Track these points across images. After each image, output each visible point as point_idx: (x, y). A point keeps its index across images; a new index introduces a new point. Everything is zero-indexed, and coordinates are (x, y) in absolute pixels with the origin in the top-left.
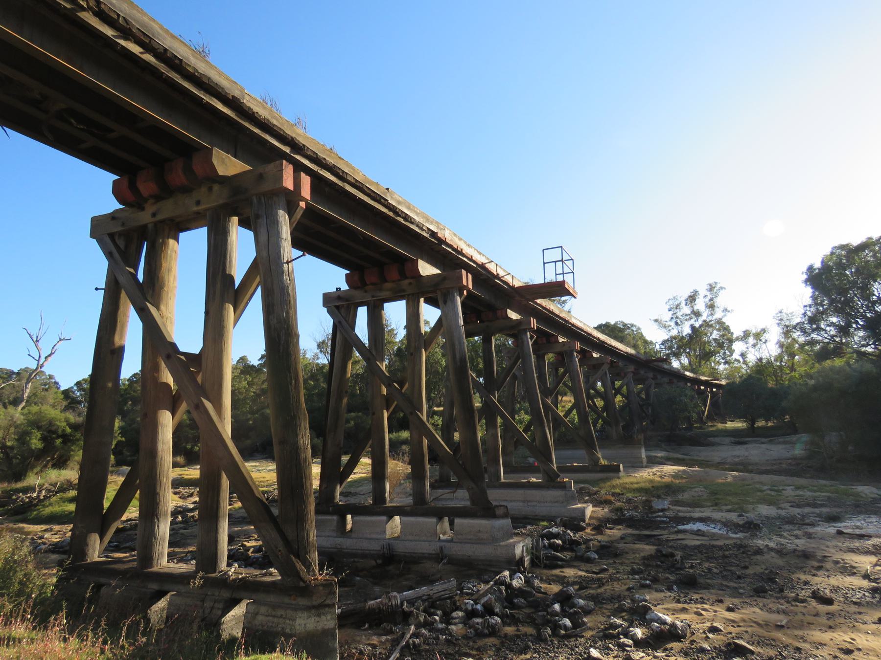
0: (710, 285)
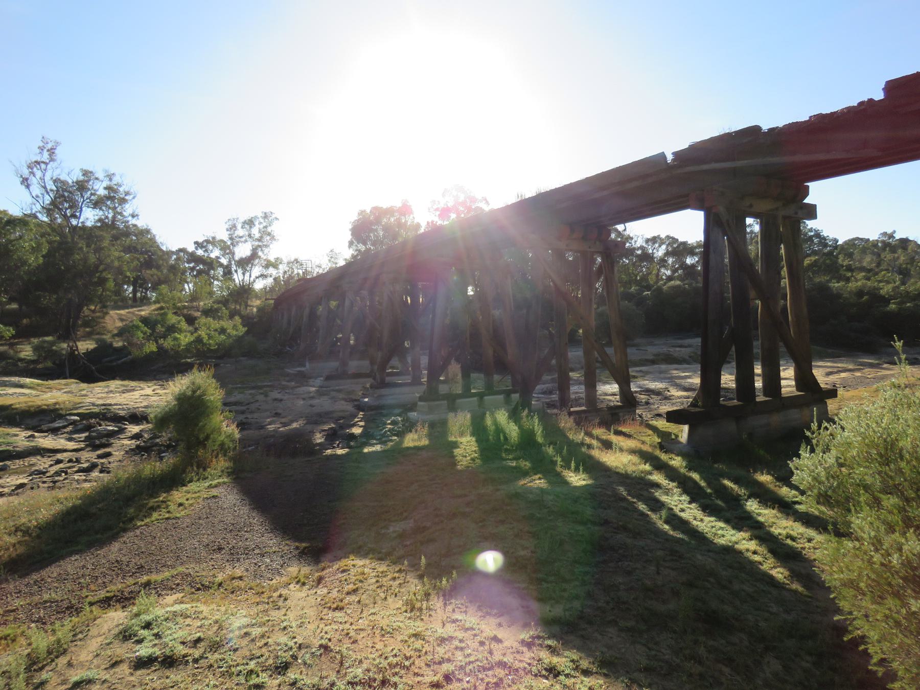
0: (265, 213)
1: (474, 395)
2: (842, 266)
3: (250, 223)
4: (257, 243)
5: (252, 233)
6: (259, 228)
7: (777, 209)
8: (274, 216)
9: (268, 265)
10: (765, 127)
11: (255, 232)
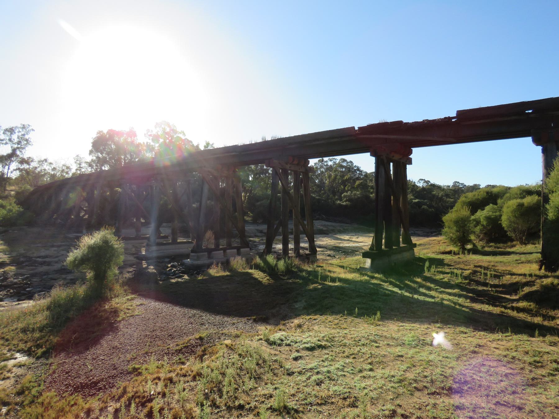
0: (24, 125)
1: (234, 248)
2: (369, 186)
3: (11, 131)
4: (16, 146)
5: (13, 138)
6: (18, 135)
7: (401, 159)
8: (30, 128)
9: (23, 161)
10: (405, 121)
11: (15, 137)
